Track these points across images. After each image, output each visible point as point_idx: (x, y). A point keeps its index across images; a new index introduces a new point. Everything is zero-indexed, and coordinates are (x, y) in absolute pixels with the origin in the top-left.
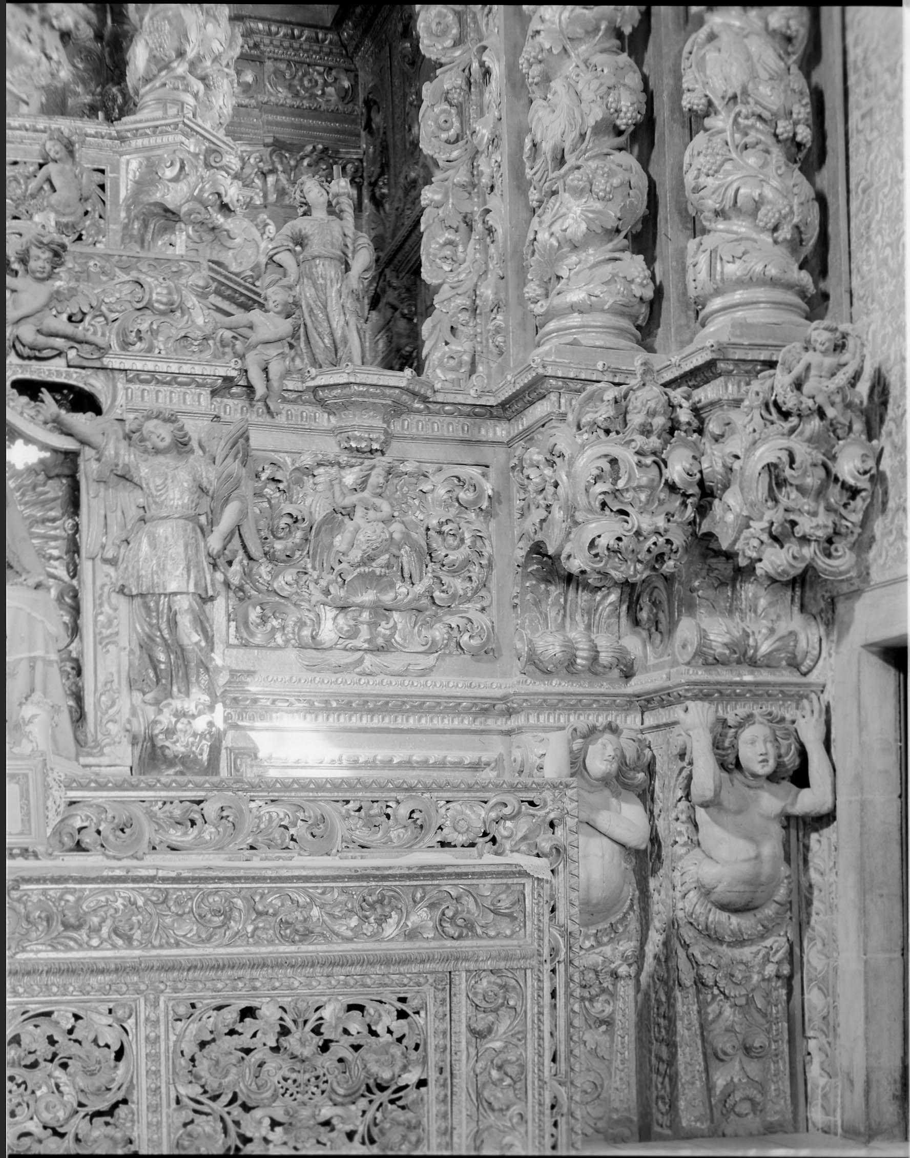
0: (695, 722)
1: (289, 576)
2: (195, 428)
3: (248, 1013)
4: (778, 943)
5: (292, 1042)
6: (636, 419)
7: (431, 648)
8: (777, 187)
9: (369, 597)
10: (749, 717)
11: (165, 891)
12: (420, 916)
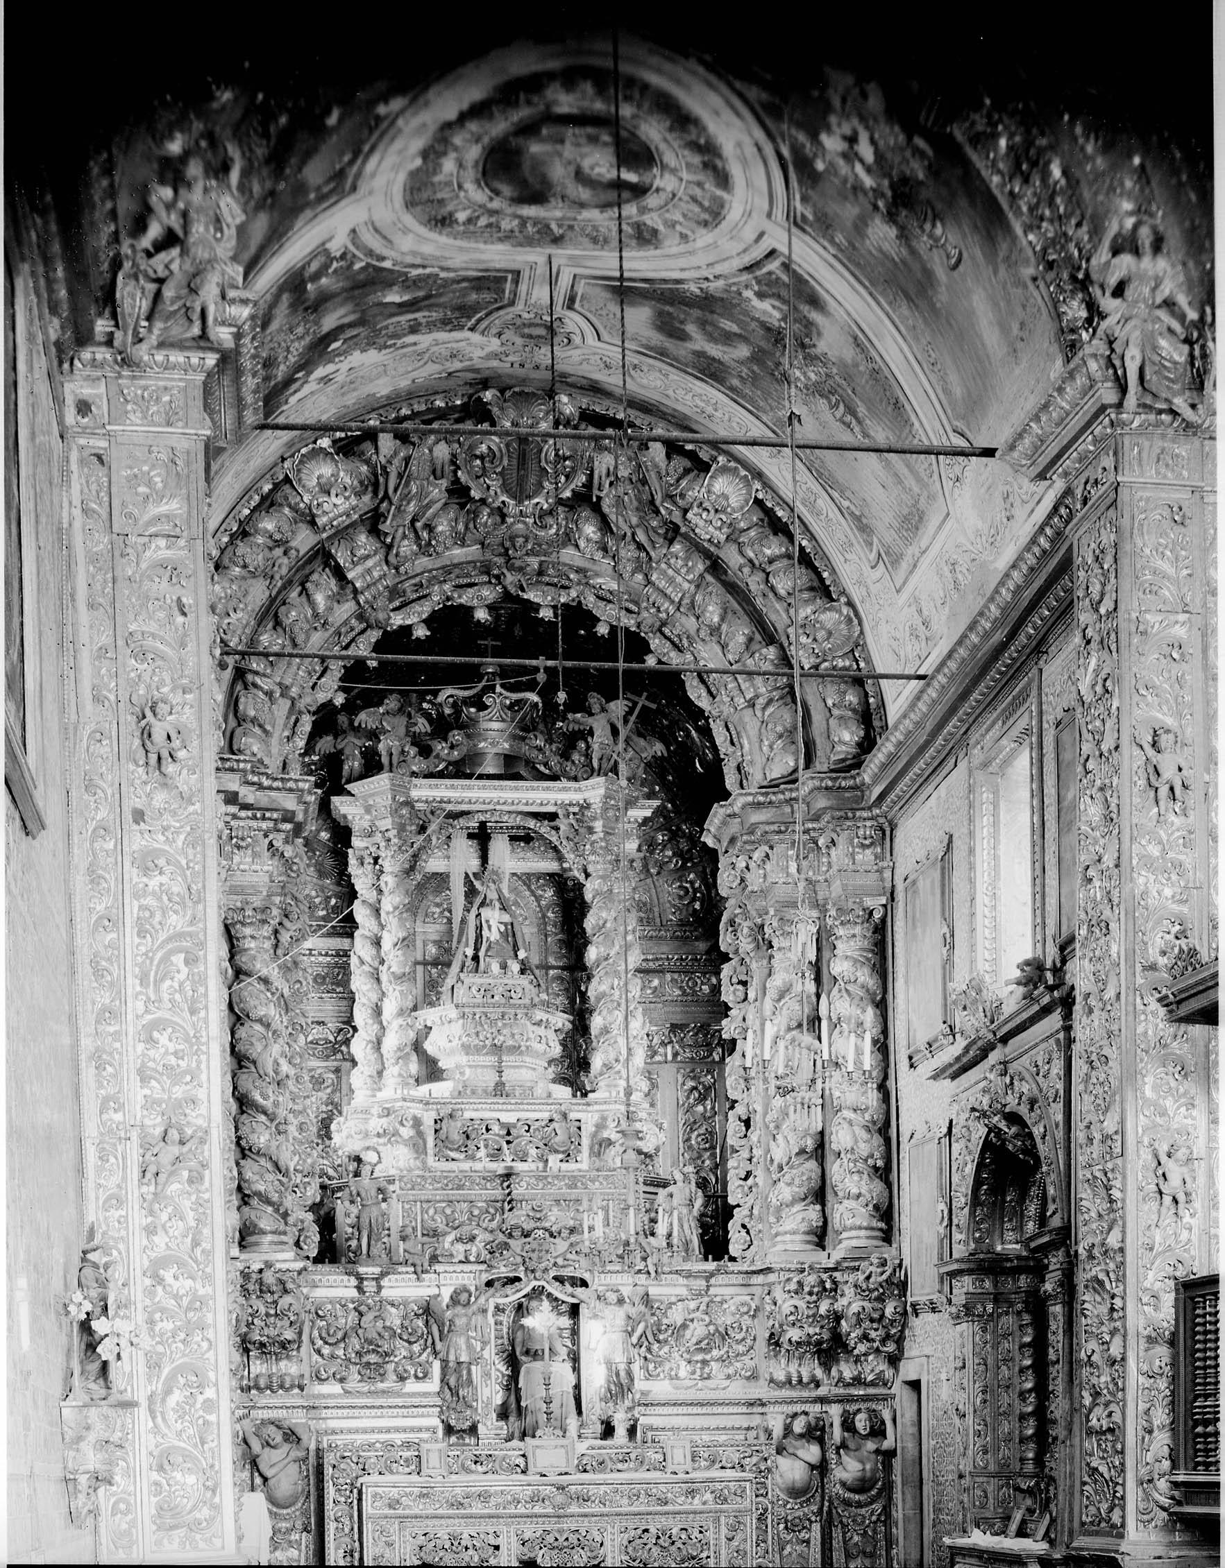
0: (835, 1411)
1: (666, 1349)
2: (626, 1291)
3: (646, 1531)
4: (878, 1507)
5: (661, 1541)
6: (807, 1289)
7: (729, 1377)
8: (872, 1189)
9: (699, 1357)
10: (859, 1410)
11: (616, 1488)
12: (708, 1496)
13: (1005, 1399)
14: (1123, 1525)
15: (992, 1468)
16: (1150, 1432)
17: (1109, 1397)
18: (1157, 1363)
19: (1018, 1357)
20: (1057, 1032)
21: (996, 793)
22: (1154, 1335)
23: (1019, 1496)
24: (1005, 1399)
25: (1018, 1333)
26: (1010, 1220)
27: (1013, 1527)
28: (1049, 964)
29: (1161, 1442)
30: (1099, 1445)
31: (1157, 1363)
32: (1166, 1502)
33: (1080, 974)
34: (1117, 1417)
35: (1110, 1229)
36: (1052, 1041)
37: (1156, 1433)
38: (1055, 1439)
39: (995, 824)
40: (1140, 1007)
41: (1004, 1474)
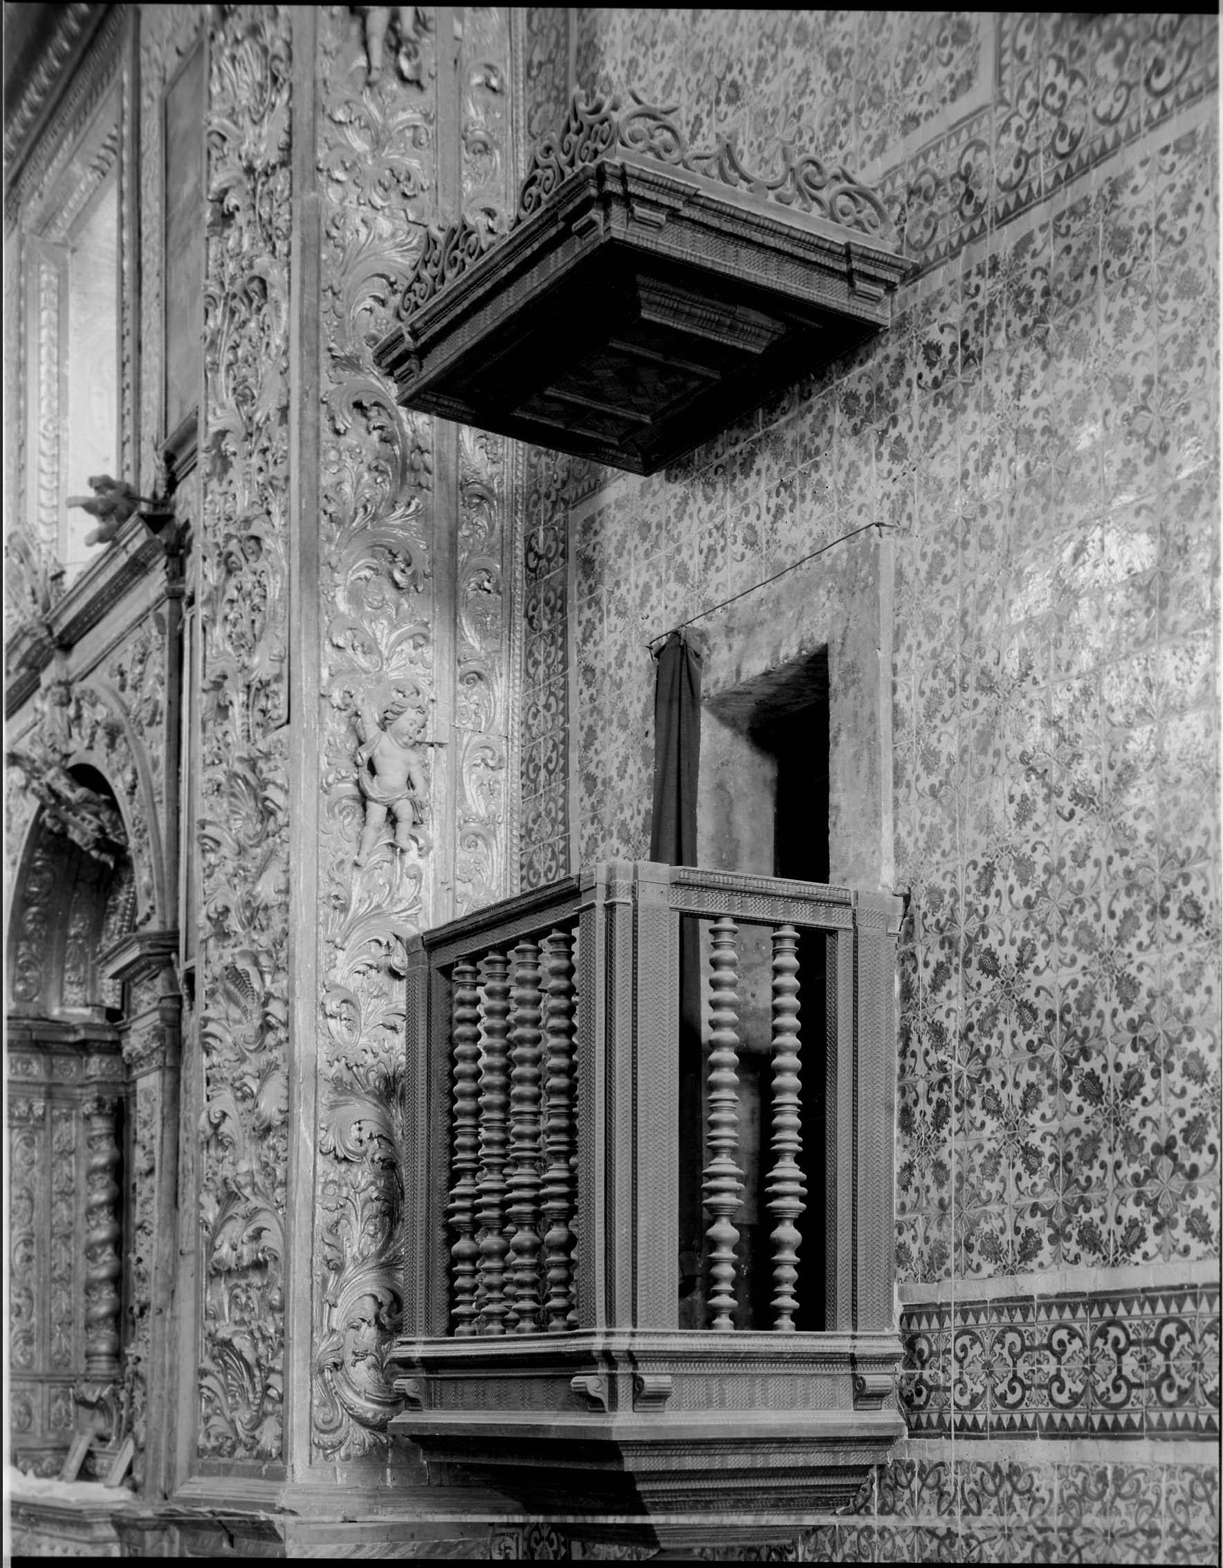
13: (63, 1256)
14: (282, 1454)
15: (40, 1366)
16: (338, 1269)
17: (255, 1202)
18: (355, 1133)
19: (83, 1186)
20: (158, 602)
21: (63, 276)
22: (347, 1077)
23: (85, 1413)
24: (63, 1256)
25: (85, 1151)
26: (75, 968)
27: (73, 1463)
28: (146, 493)
29: (359, 1291)
30: (234, 1298)
31: (355, 1133)
32: (368, 1409)
33: (195, 503)
34: (271, 1240)
35: (262, 870)
36: (151, 621)
37: (349, 1271)
38: (144, 1308)
39: (61, 325)
40: (327, 435)
41: (59, 1377)
